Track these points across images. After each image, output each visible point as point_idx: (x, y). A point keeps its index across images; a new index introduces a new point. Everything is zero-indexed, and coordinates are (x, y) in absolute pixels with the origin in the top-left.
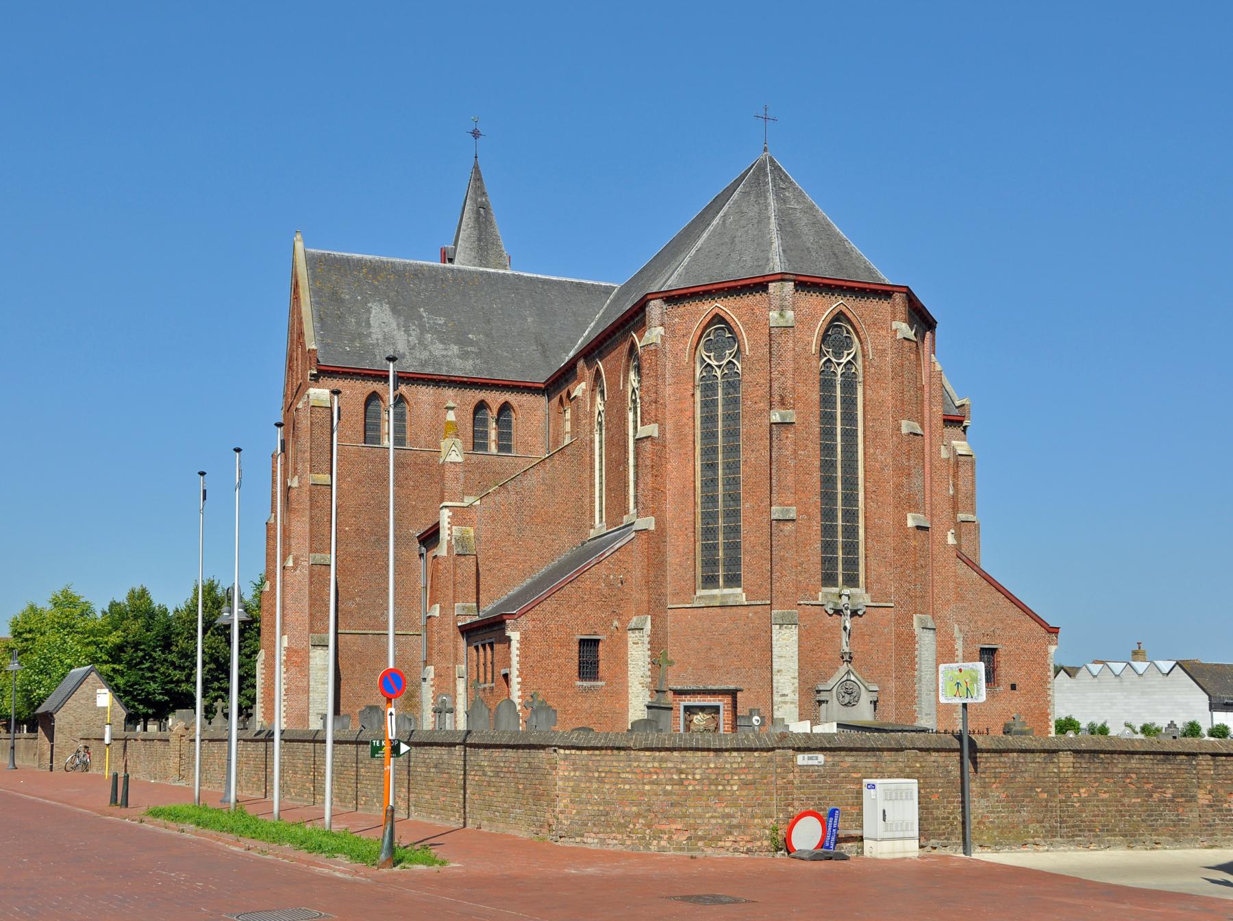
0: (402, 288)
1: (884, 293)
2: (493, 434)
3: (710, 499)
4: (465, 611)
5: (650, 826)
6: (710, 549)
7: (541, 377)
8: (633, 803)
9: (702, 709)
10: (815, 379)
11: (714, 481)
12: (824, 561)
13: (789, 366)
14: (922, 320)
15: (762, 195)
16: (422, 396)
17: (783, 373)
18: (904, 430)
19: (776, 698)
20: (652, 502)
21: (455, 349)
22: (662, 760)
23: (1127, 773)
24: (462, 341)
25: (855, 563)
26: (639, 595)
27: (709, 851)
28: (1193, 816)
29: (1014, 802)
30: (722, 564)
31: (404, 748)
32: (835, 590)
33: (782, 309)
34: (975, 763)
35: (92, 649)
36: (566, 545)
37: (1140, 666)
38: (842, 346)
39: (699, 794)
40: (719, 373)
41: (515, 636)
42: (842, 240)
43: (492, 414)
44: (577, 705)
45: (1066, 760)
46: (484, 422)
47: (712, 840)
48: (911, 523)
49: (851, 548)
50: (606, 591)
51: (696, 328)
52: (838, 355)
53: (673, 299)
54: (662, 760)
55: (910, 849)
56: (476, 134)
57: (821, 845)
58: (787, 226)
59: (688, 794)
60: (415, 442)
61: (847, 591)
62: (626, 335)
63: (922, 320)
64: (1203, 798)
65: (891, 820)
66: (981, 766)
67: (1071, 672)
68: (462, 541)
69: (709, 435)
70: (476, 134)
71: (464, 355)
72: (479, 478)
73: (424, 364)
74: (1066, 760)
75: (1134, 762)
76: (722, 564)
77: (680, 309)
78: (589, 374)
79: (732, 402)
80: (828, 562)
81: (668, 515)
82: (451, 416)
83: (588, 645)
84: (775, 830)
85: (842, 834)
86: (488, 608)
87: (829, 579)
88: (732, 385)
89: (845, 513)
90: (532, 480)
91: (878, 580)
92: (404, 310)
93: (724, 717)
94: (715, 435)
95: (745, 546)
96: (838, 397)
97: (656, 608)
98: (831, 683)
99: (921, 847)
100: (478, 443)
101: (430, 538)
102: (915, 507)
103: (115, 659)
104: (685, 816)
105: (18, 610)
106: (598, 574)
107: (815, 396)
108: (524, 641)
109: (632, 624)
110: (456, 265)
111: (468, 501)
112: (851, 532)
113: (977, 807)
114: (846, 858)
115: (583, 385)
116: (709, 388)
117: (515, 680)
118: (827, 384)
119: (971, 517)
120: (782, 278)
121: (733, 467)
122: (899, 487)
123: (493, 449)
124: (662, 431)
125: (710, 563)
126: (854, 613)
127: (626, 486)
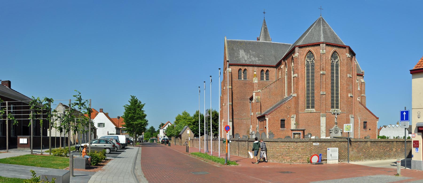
0: (247, 46)
1: (344, 47)
2: (265, 77)
3: (308, 90)
4: (258, 114)
5: (282, 158)
6: (308, 100)
7: (275, 64)
8: (279, 153)
9: (297, 134)
10: (330, 65)
11: (309, 86)
12: (332, 103)
13: (324, 62)
14: (352, 54)
15: (320, 25)
16: (250, 69)
17: (323, 63)
18: (348, 76)
19: (321, 132)
20: (296, 91)
21: (257, 59)
22: (285, 144)
23: (381, 145)
24: (258, 57)
25: (338, 104)
26: (293, 110)
27: (295, 163)
28: (392, 153)
29: (358, 152)
30: (310, 104)
31: (230, 141)
32: (334, 109)
33: (323, 50)
34: (351, 144)
35: (190, 123)
36: (279, 99)
37: (397, 126)
38: (336, 58)
39: (292, 151)
40: (310, 63)
41: (267, 119)
42: (336, 36)
43: (265, 72)
44: (282, 133)
45: (369, 143)
46: (263, 74)
47: (295, 161)
48: (349, 96)
49: (337, 101)
50: (286, 109)
51: (305, 53)
52: (335, 60)
53: (300, 47)
54: (285, 144)
55: (337, 162)
56: (264, 13)
57: (318, 161)
58: (325, 32)
59: (290, 151)
60: (249, 79)
61: (336, 110)
62: (291, 55)
63: (352, 54)
64: (394, 150)
65: (333, 156)
66: (352, 145)
67: (385, 127)
68: (257, 99)
69: (308, 76)
70: (264, 13)
71: (259, 60)
72: (261, 86)
73: (250, 62)
74: (369, 143)
75: (382, 143)
76: (310, 104)
77: (302, 49)
78: (284, 63)
79: (313, 69)
80: (332, 103)
81: (300, 93)
82: (255, 73)
83: (283, 121)
84: (308, 158)
85: (323, 159)
86: (263, 113)
87: (333, 107)
88: (313, 66)
89: (336, 93)
90: (272, 86)
91: (343, 107)
92: (247, 51)
93: (302, 135)
94: (309, 76)
95: (315, 100)
96: (334, 69)
97: (297, 113)
98: (333, 129)
99: (339, 161)
100: (262, 78)
101: (251, 99)
102: (350, 92)
103: (194, 125)
104: (290, 156)
105: (176, 115)
106: (285, 105)
107: (330, 68)
108: (269, 120)
109: (292, 116)
110: (260, 41)
111: (259, 91)
112: (337, 97)
113: (351, 153)
114: (322, 164)
115: (283, 66)
116: (308, 66)
117: (267, 128)
118: (332, 66)
119: (364, 95)
120: (323, 43)
121: (313, 83)
122: (347, 88)
123: (265, 80)
124: (298, 75)
125: (308, 103)
126: (338, 114)
127: (291, 87)
